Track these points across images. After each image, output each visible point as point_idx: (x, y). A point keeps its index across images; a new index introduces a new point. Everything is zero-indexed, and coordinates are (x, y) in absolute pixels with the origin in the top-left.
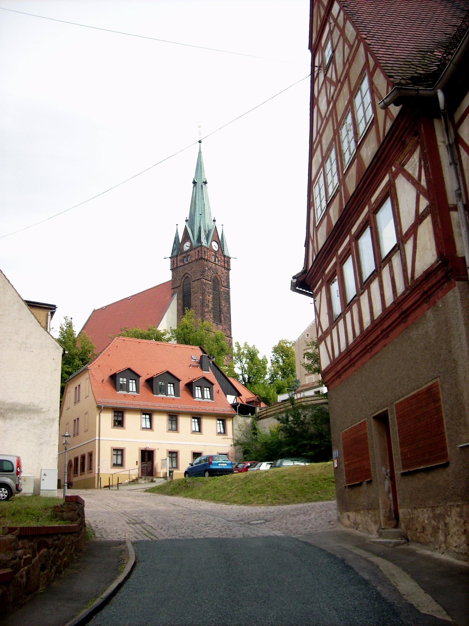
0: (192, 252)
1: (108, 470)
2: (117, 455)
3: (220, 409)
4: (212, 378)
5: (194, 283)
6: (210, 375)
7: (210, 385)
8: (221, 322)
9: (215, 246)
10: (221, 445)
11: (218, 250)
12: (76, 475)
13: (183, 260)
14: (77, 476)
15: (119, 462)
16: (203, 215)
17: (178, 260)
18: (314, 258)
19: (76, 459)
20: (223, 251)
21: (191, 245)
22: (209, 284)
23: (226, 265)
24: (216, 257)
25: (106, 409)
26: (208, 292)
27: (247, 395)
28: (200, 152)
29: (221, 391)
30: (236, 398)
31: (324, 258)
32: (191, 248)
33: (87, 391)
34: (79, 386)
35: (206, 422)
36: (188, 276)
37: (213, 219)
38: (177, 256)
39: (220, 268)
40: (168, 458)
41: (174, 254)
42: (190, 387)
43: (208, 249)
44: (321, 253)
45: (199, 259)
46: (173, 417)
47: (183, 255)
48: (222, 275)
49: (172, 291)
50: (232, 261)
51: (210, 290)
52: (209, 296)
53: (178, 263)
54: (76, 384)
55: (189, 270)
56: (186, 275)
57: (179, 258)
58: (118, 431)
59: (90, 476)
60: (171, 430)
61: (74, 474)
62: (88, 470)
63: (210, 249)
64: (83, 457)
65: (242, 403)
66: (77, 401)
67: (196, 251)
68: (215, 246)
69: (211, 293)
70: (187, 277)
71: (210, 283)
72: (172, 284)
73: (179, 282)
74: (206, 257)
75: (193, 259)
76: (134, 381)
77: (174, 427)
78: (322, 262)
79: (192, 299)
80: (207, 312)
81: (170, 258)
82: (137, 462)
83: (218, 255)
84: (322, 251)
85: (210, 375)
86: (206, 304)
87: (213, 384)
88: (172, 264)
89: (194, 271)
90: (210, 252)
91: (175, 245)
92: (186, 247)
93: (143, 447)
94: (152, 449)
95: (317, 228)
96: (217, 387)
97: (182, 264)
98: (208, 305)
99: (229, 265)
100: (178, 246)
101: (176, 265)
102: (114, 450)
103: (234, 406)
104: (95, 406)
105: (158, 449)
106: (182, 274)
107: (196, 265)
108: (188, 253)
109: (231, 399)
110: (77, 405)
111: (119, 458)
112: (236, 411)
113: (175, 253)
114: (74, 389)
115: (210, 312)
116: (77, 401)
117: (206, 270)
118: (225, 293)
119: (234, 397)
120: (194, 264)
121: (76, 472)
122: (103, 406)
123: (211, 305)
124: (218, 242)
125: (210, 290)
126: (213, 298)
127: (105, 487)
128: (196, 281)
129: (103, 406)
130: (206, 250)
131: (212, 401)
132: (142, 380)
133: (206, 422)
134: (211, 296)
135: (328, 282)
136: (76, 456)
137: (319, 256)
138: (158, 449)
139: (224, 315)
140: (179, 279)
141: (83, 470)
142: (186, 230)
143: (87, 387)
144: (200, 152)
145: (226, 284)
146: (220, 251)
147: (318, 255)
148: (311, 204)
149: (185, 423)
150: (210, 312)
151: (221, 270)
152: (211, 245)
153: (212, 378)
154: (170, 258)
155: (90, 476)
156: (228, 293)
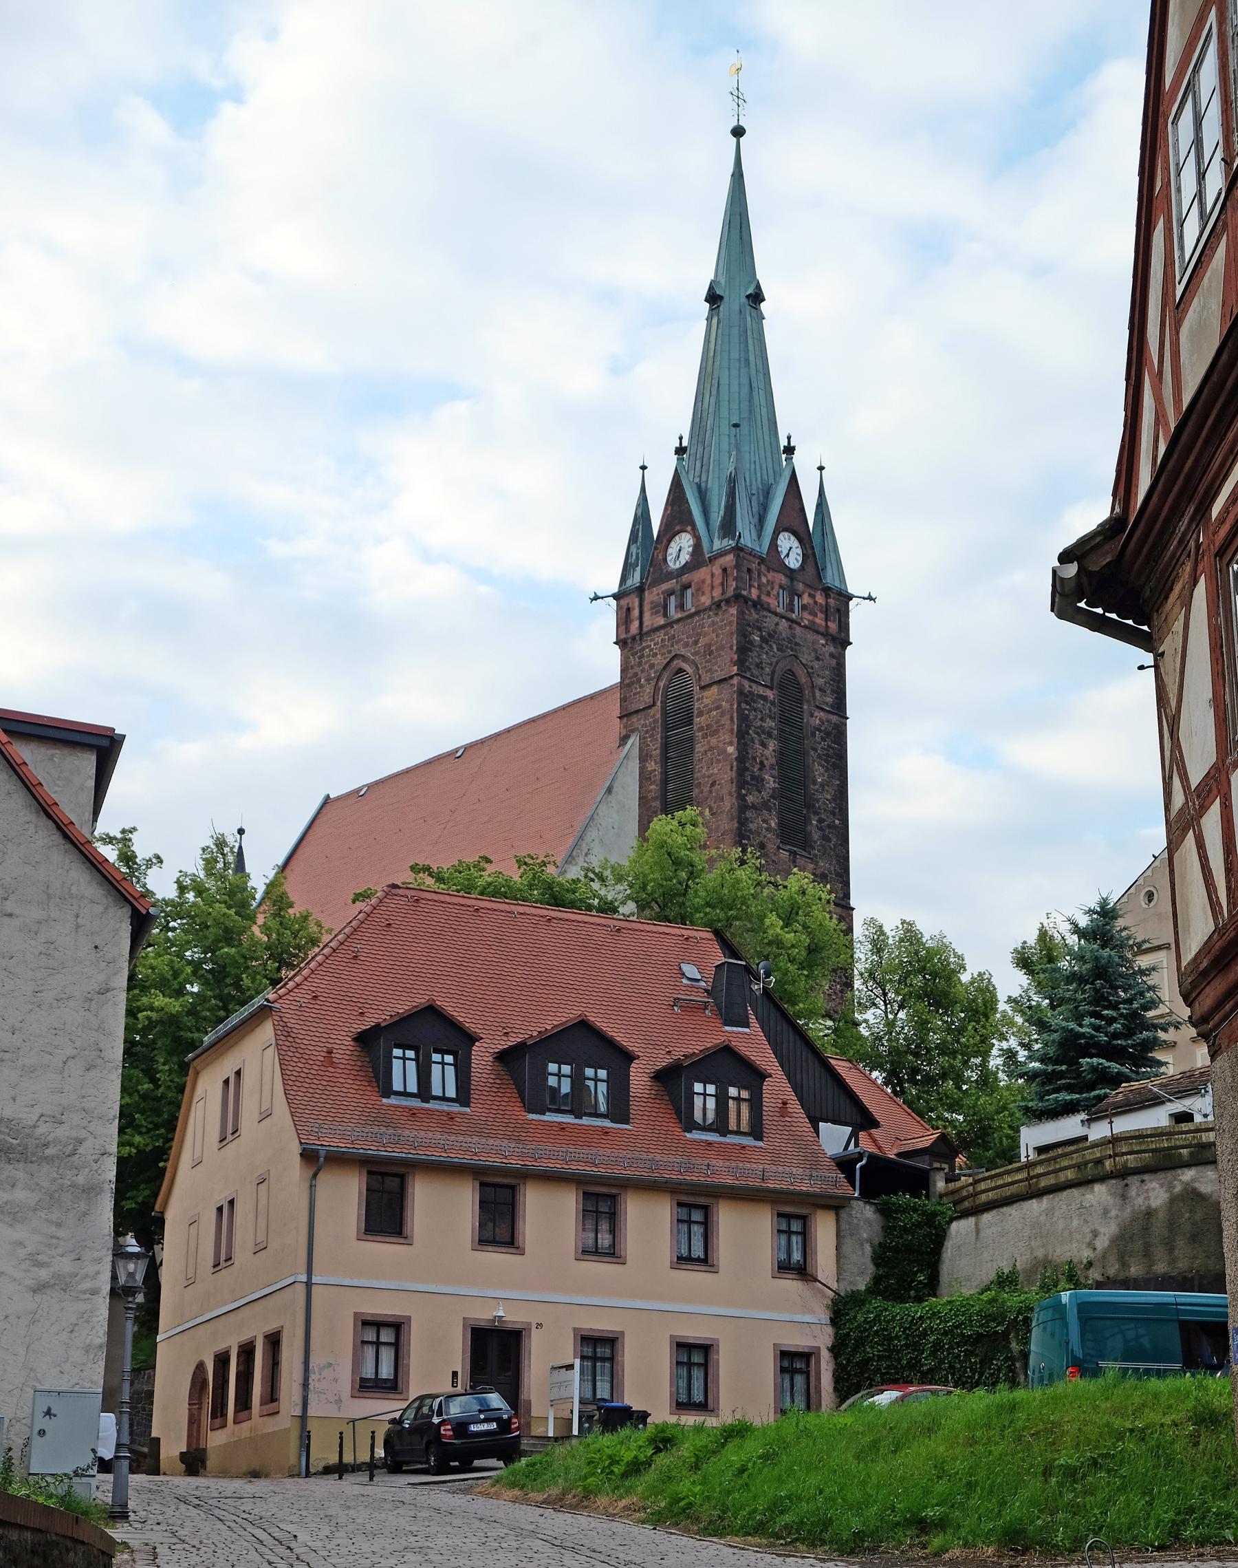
0: (703, 573)
1: (339, 1402)
2: (378, 1344)
3: (795, 1177)
4: (761, 1054)
5: (708, 693)
6: (752, 1042)
7: (754, 1077)
8: (806, 844)
9: (791, 550)
10: (788, 1317)
11: (802, 567)
12: (218, 1421)
13: (665, 607)
14: (224, 1426)
15: (386, 1372)
16: (745, 428)
17: (646, 608)
18: (1162, 449)
19: (222, 1360)
20: (819, 573)
21: (697, 547)
22: (765, 698)
23: (833, 627)
24: (794, 593)
25: (338, 1160)
26: (761, 731)
27: (901, 1132)
28: (738, 176)
29: (795, 1106)
30: (854, 1135)
31: (1207, 442)
32: (698, 558)
33: (267, 1088)
34: (238, 1073)
35: (727, 1218)
36: (685, 666)
37: (783, 442)
38: (640, 590)
39: (811, 636)
40: (577, 1362)
41: (629, 583)
42: (672, 1080)
43: (762, 560)
44: (1194, 417)
45: (728, 601)
46: (601, 1202)
47: (665, 586)
48: (816, 665)
49: (616, 727)
50: (857, 610)
51: (770, 724)
52: (764, 745)
53: (647, 616)
54: (226, 1067)
55: (686, 645)
56: (678, 663)
57: (651, 596)
58: (383, 1250)
59: (273, 1425)
60: (591, 1252)
61: (214, 1417)
62: (263, 1403)
63: (773, 559)
64: (247, 1351)
65: (875, 1150)
66: (229, 1131)
67: (717, 570)
68: (791, 550)
69: (770, 735)
70: (681, 670)
71: (770, 694)
72: (623, 700)
73: (649, 689)
74: (754, 593)
75: (706, 600)
76: (449, 1059)
77: (605, 1240)
78: (1196, 461)
79: (697, 756)
80: (754, 807)
81: (615, 596)
82: (455, 1374)
83: (800, 587)
84: (1199, 406)
85: (752, 1042)
86: (753, 778)
87: (762, 1076)
88: (624, 619)
89: (708, 646)
90: (771, 575)
91: (634, 549)
92: (681, 549)
93: (484, 1314)
94: (407, 1230)
95: (1176, 309)
96: (777, 1087)
97: (662, 621)
98: (759, 782)
99: (844, 627)
100: (645, 547)
101: (636, 624)
102: (366, 1323)
103: (845, 1164)
104: (296, 1149)
105: (539, 1325)
106: (660, 661)
107: (713, 624)
108: (685, 578)
109: (835, 1137)
110: (231, 1148)
111: (387, 1355)
112: (852, 1183)
113: (635, 579)
114: (219, 1086)
115: (766, 805)
116: (229, 1131)
117: (751, 642)
118: (828, 734)
119: (848, 1130)
120: (706, 620)
121: (219, 1410)
122: (322, 1154)
123: (770, 782)
124: (803, 535)
125: (770, 724)
126: (781, 755)
127: (327, 1470)
128: (715, 689)
129: (322, 1154)
130: (754, 566)
131: (760, 1144)
132: (481, 1057)
133: (727, 1218)
134: (772, 745)
135: (1220, 554)
136: (220, 1347)
137: (1184, 437)
138: (539, 1325)
139: (821, 821)
140: (648, 680)
141: (244, 1403)
142: (676, 484)
143: (267, 1077)
144: (738, 176)
145: (829, 700)
146: (810, 569)
147: (1180, 428)
148: (1157, 204)
149: (648, 1223)
150: (766, 805)
151: (815, 642)
152: (774, 544)
153: (761, 1054)
154: (615, 596)
155: (273, 1425)
156: (838, 736)
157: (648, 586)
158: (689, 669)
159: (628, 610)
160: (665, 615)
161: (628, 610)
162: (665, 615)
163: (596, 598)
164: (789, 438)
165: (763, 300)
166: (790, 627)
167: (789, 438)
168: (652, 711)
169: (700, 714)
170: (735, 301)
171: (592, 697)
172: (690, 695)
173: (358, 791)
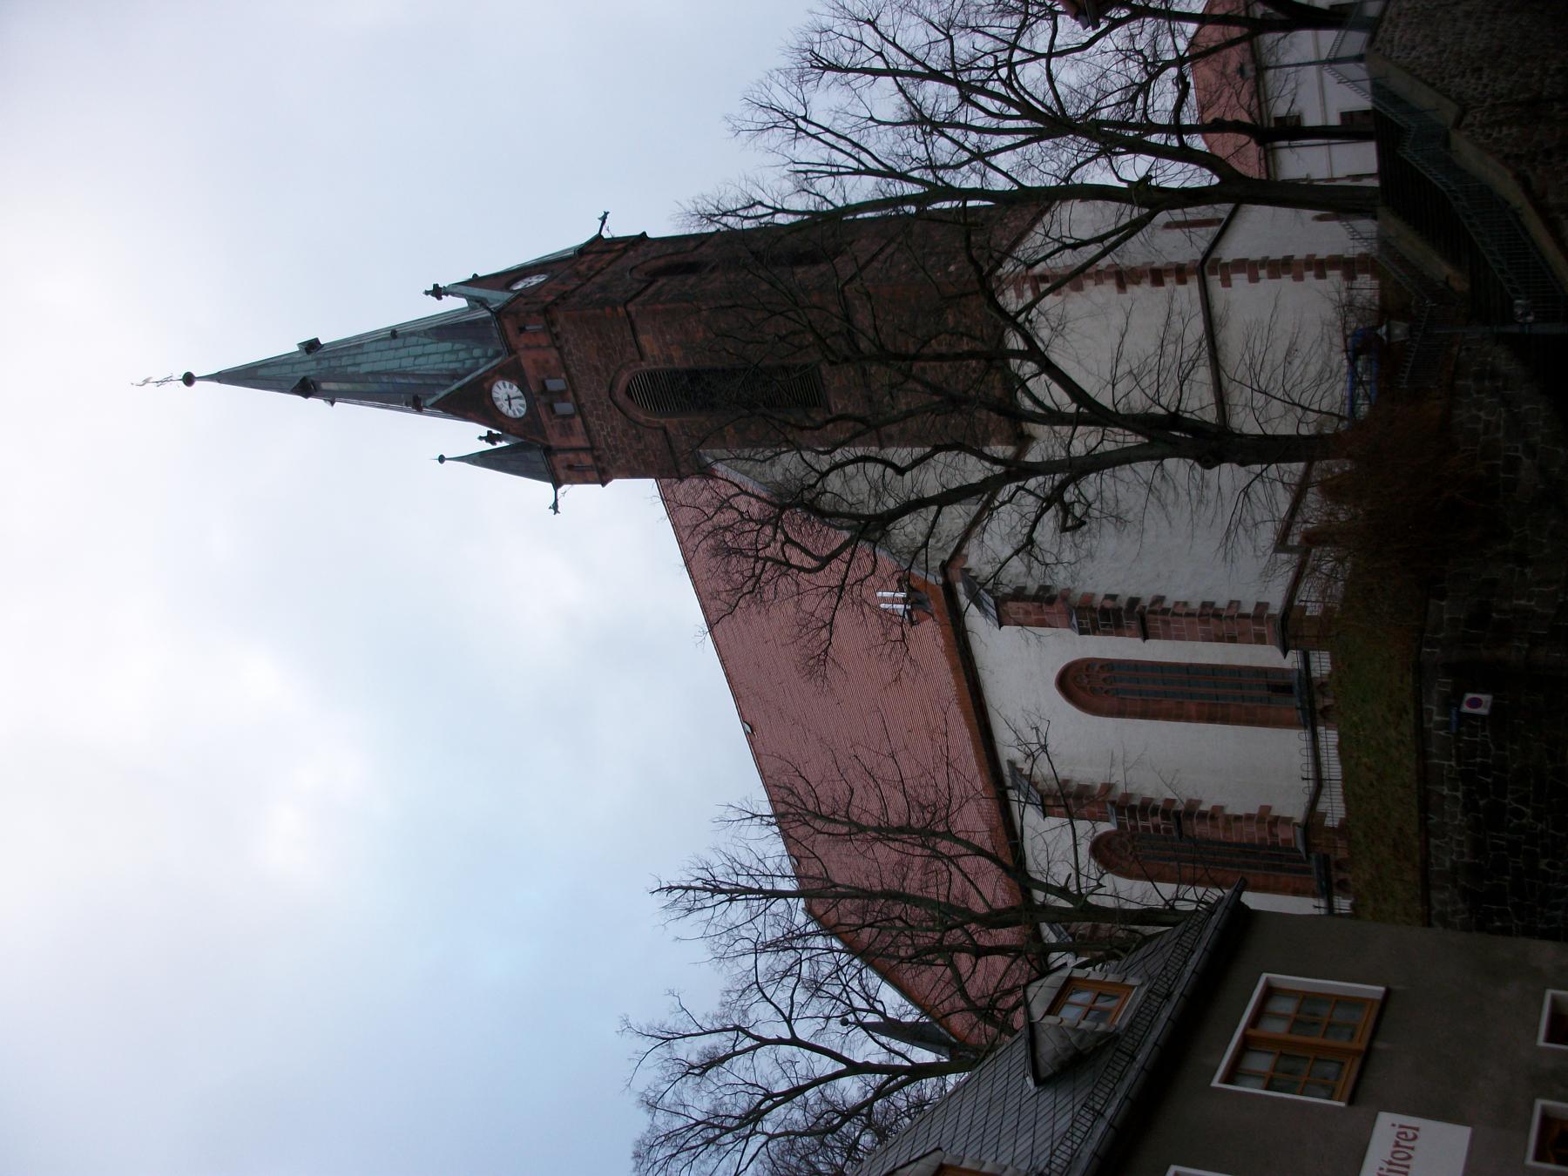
17: (567, 444)
81: (556, 487)
92: (508, 398)
97: (578, 419)
154: (556, 487)
157: (544, 447)
158: (624, 379)
159: (570, 467)
160: (572, 416)
161: (570, 467)
162: (572, 416)
163: (555, 507)
164: (437, 292)
165: (316, 340)
166: (1220, 220)
167: (437, 292)
168: (672, 431)
169: (670, 359)
170: (314, 372)
171: (729, 682)
172: (652, 375)
173: (747, 733)
